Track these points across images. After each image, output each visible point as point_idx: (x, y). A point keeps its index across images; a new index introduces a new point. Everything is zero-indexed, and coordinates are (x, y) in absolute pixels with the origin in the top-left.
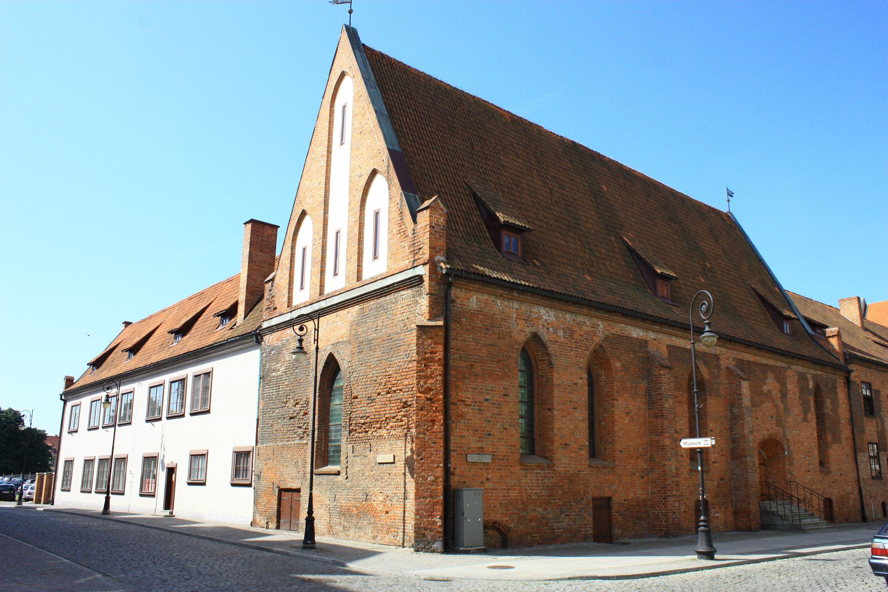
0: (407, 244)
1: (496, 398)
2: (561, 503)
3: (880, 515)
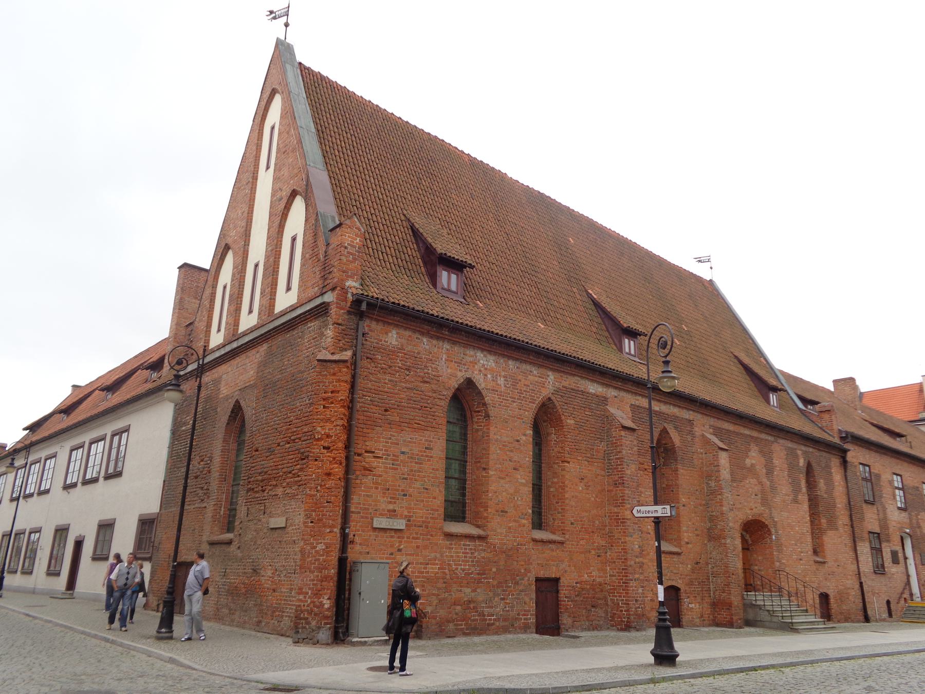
0: (317, 269)
1: (416, 451)
2: (495, 583)
3: (885, 615)
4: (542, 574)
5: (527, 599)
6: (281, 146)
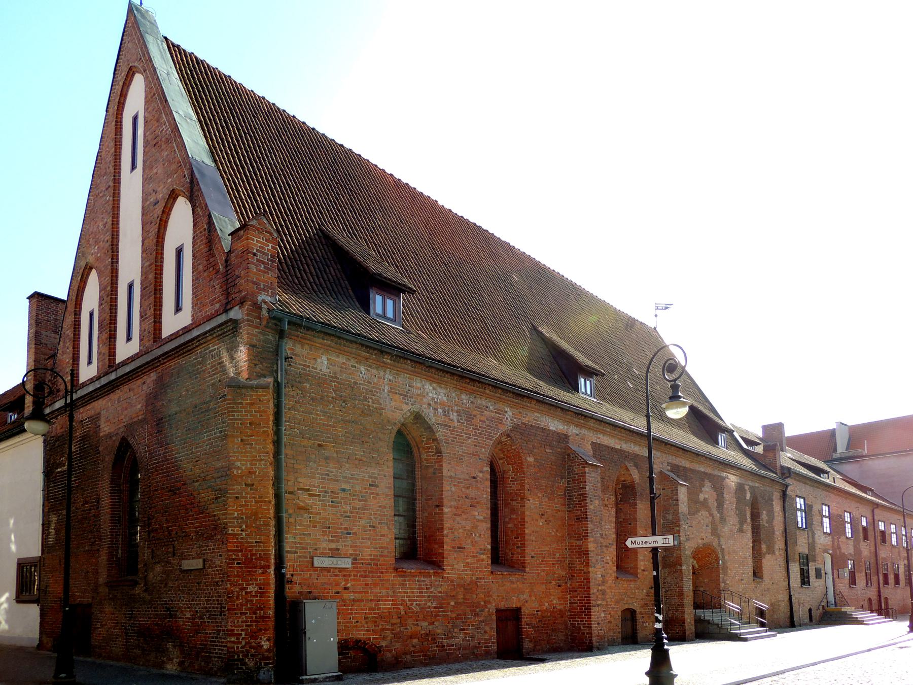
4: (503, 605)
5: (487, 628)
6: (149, 138)
